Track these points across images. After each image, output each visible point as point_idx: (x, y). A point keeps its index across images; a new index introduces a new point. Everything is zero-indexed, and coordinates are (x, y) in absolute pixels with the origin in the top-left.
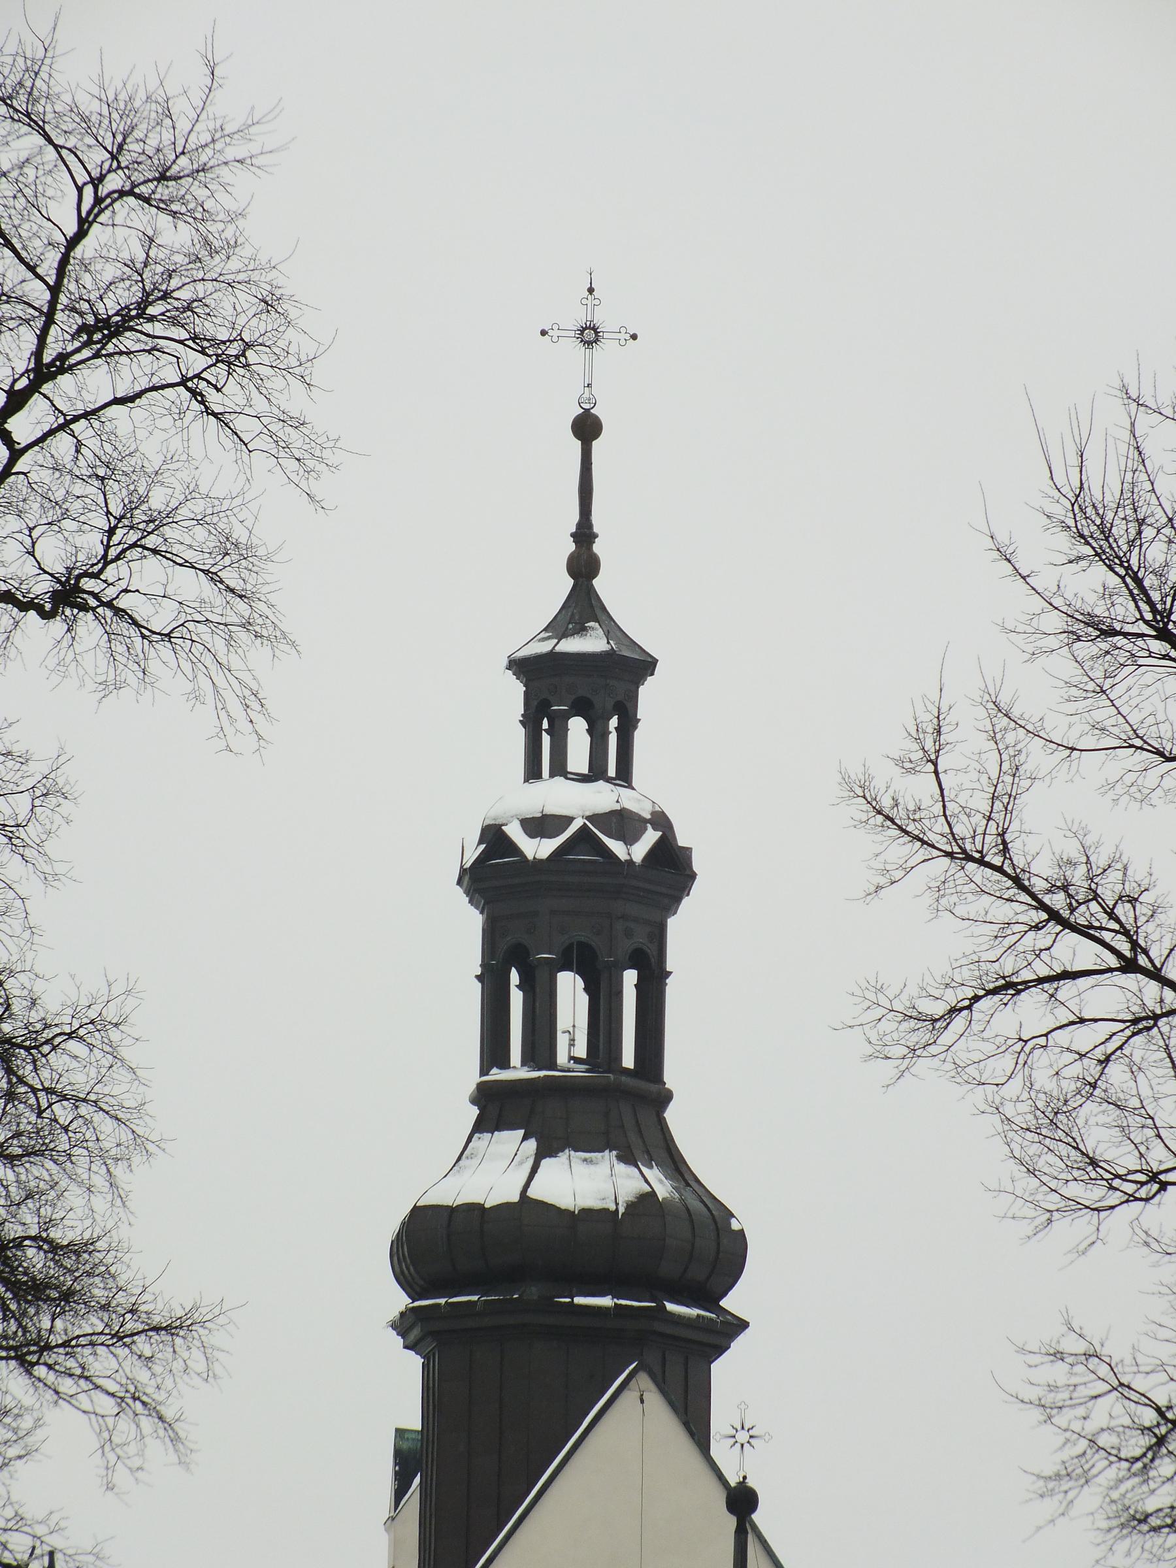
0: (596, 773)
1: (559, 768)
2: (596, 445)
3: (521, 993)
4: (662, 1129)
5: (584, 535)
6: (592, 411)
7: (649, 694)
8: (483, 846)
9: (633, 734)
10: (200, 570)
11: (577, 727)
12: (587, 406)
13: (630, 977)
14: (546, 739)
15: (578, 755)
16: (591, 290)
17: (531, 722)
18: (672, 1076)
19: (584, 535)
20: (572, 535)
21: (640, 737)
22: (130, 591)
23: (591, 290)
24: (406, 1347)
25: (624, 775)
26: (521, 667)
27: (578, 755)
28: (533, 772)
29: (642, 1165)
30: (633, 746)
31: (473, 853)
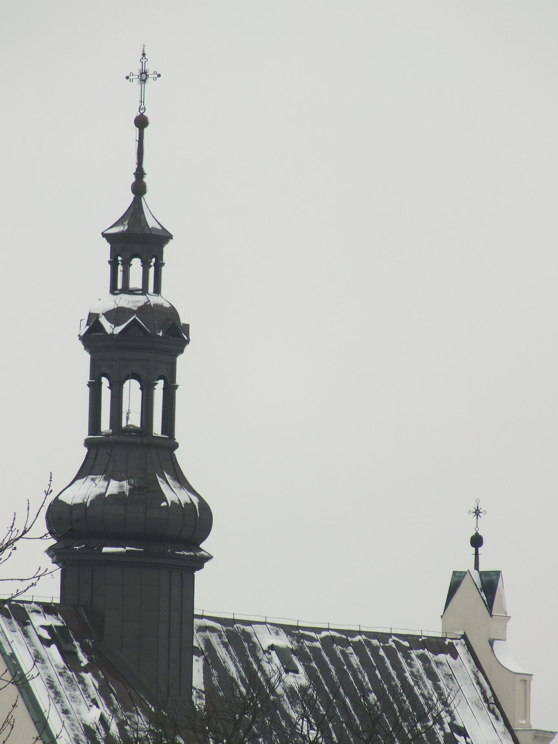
0: (144, 291)
1: (126, 290)
2: (146, 130)
3: (110, 390)
4: (175, 470)
5: (140, 173)
6: (144, 114)
7: (168, 250)
8: (88, 327)
9: (175, 391)
10: (23, 534)
11: (136, 264)
12: (142, 111)
13: (160, 384)
14: (120, 268)
15: (136, 282)
16: (144, 55)
17: (114, 264)
18: (179, 436)
19: (140, 173)
20: (163, 388)
21: (164, 269)
22: (34, 665)
23: (144, 55)
24: (53, 563)
25: (157, 290)
26: (108, 237)
27: (136, 282)
28: (113, 290)
29: (167, 473)
30: (175, 403)
31: (84, 329)
